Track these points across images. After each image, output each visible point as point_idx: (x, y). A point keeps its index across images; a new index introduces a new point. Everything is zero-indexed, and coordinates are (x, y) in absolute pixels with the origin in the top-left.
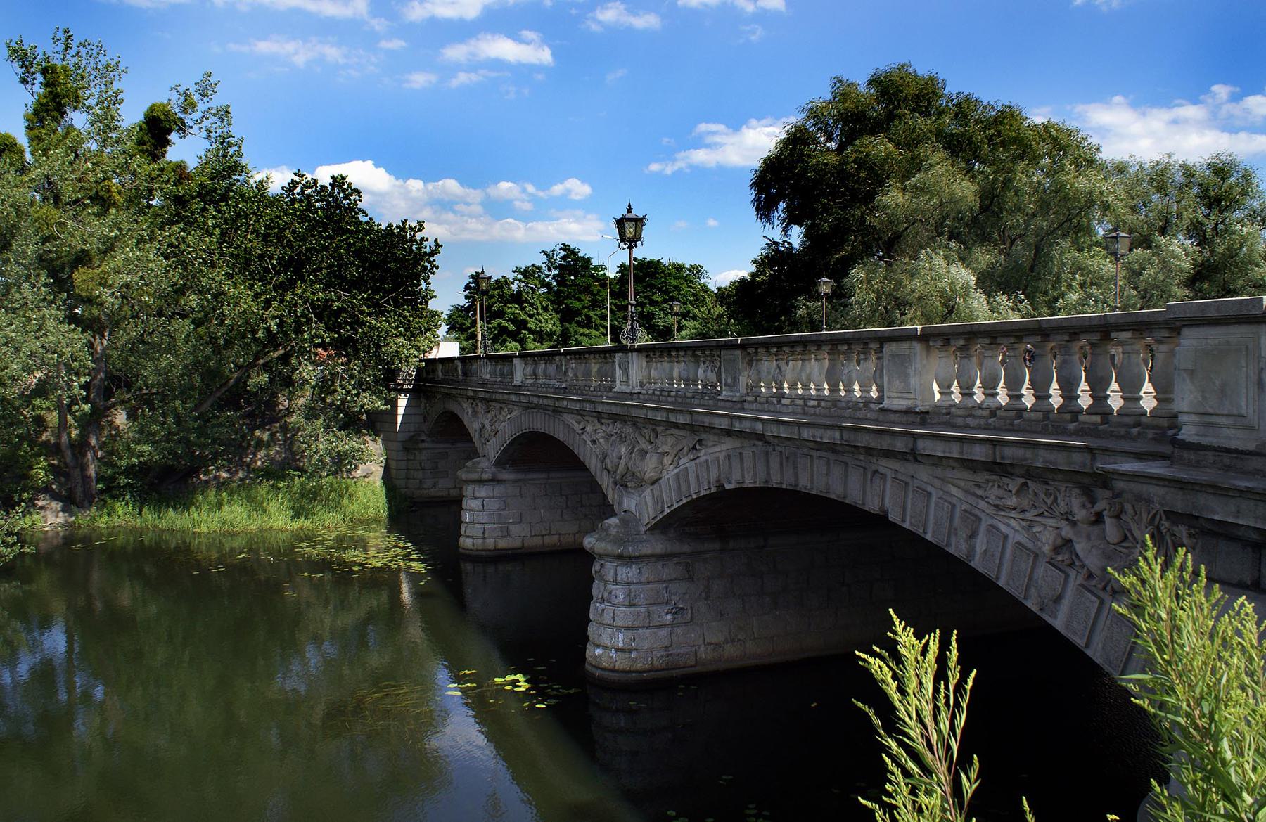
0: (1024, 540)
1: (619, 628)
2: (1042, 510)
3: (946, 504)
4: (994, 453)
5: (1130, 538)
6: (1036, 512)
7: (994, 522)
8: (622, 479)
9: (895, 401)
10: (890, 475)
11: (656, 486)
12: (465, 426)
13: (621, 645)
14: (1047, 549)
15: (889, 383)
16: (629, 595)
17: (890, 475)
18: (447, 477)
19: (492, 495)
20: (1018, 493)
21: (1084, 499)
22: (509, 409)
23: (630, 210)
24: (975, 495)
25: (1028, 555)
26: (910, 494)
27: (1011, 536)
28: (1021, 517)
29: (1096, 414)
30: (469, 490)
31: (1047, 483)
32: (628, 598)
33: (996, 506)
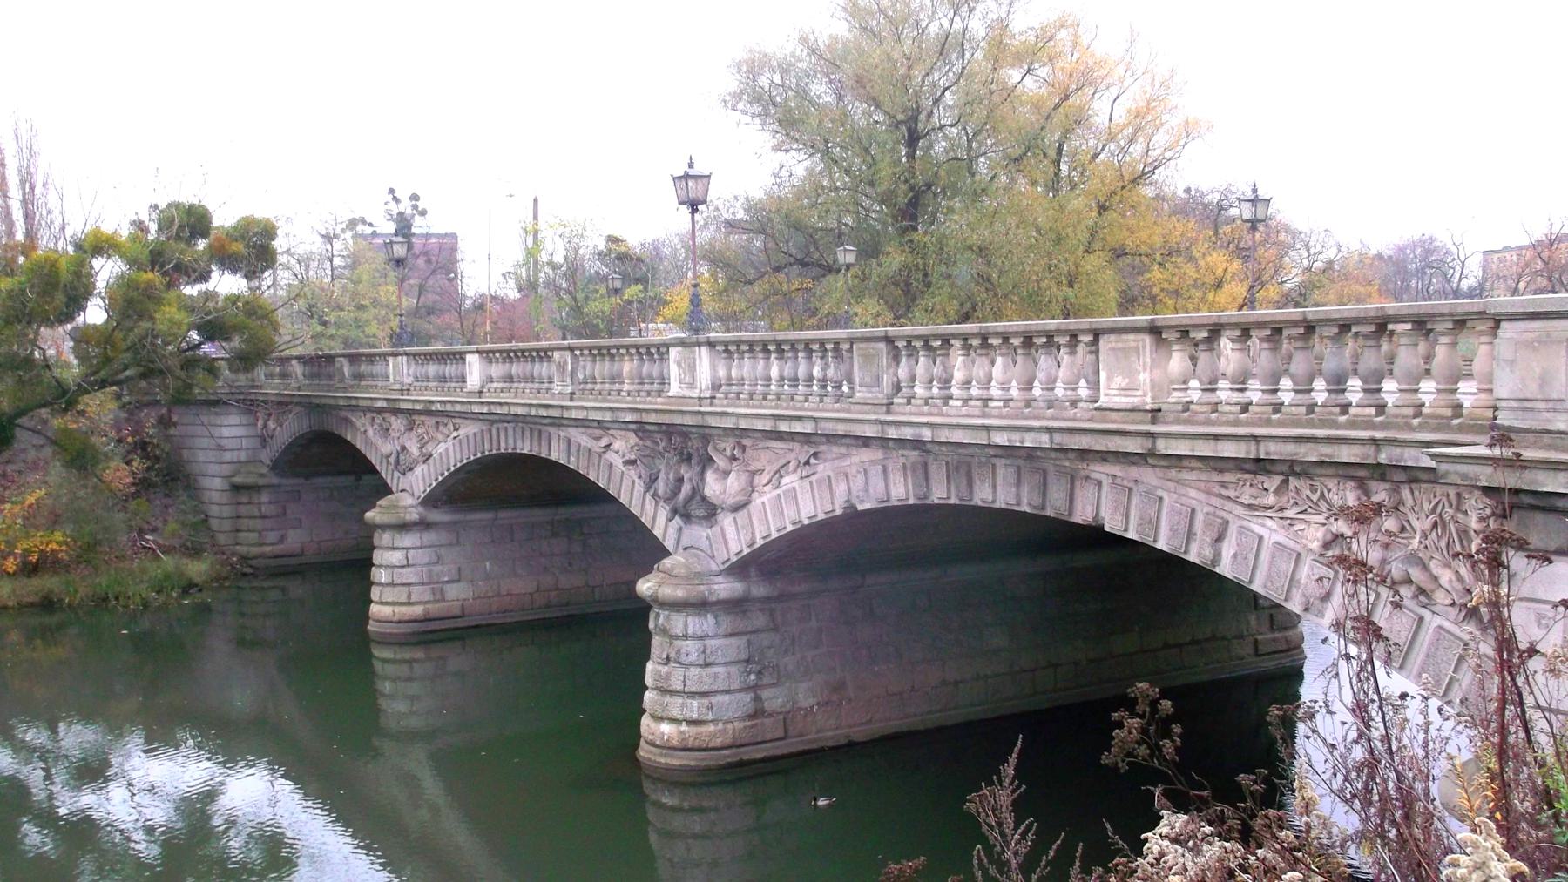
0: (1282, 540)
1: (692, 695)
2: (1306, 507)
3: (1185, 508)
4: (1258, 450)
5: (1408, 527)
6: (1299, 509)
7: (1245, 523)
8: (684, 506)
9: (1117, 399)
10: (1106, 481)
11: (743, 513)
12: (359, 452)
13: (694, 716)
14: (1315, 545)
15: (1109, 379)
16: (704, 652)
17: (1106, 481)
18: (300, 527)
19: (418, 544)
20: (1277, 492)
21: (1359, 492)
22: (454, 425)
23: (691, 165)
24: (1221, 496)
25: (1290, 554)
26: (1135, 501)
27: (1266, 537)
28: (1280, 515)
29: (1371, 406)
30: (384, 538)
31: (1312, 479)
32: (702, 656)
33: (1250, 507)
